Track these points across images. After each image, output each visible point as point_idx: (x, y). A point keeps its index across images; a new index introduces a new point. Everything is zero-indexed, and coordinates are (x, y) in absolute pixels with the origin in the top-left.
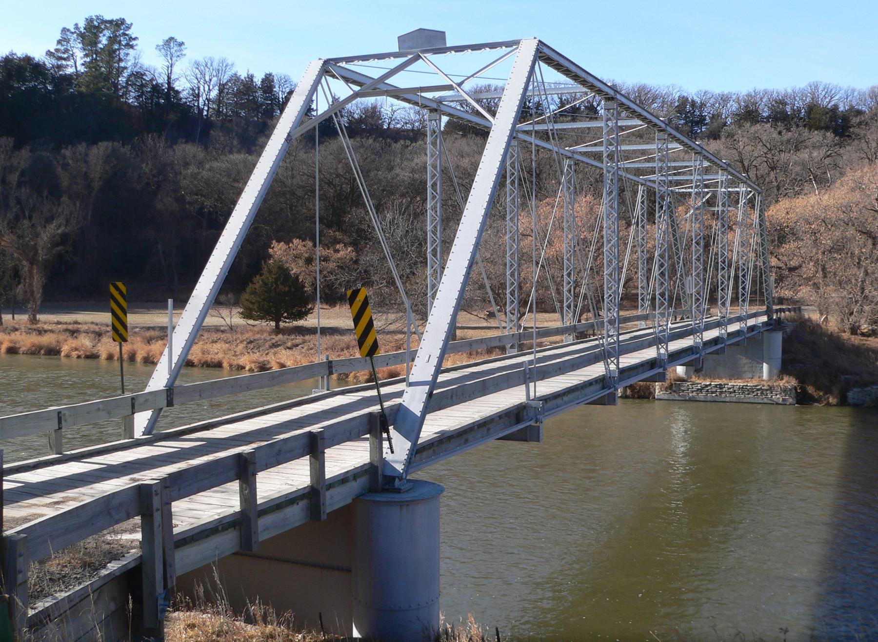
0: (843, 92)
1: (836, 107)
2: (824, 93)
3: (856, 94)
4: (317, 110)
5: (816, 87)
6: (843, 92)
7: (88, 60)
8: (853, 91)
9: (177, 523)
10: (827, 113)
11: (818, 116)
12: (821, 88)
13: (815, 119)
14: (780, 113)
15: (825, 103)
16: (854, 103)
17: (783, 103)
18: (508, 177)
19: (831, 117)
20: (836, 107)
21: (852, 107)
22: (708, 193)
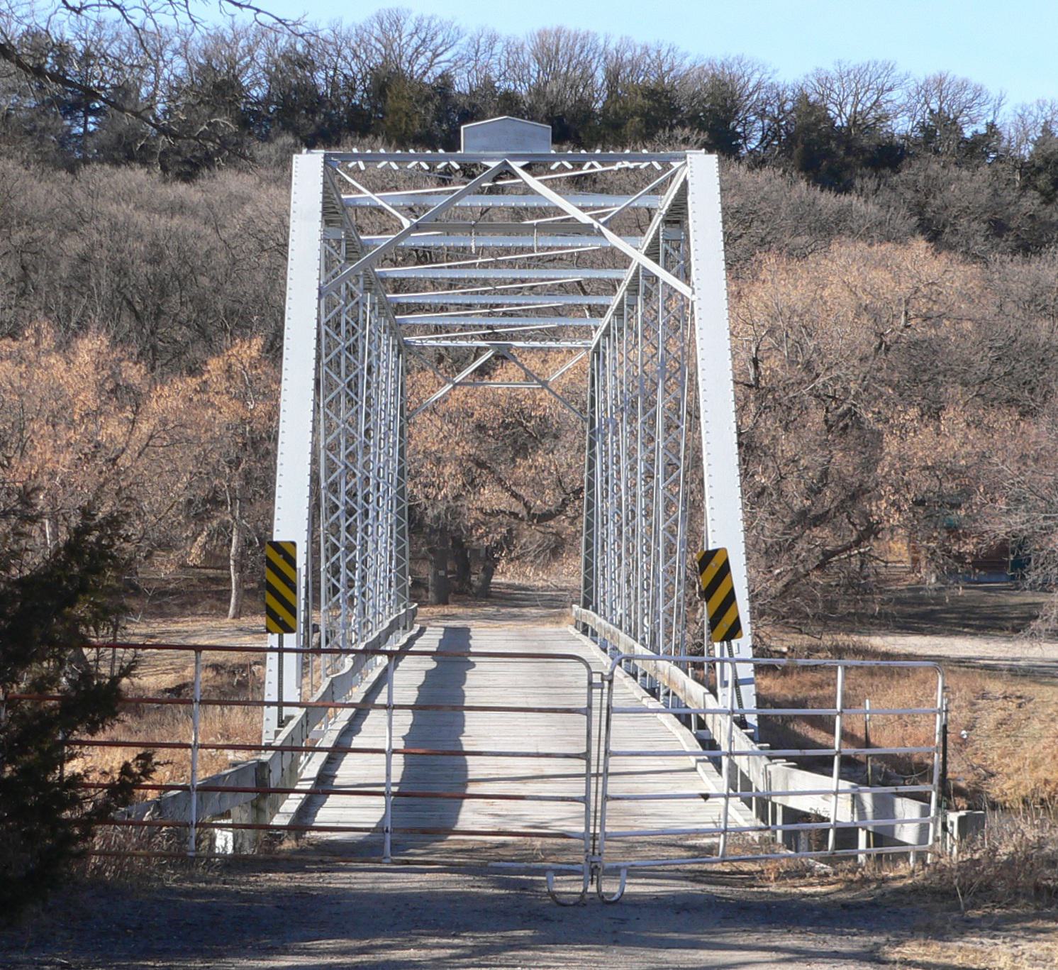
0: (463, 41)
1: (445, 82)
2: (415, 41)
3: (498, 48)
4: (186, 24)
5: (397, 23)
6: (463, 41)
7: (394, 143)
8: (493, 40)
9: (235, 711)
10: (429, 98)
11: (404, 105)
12: (409, 27)
13: (396, 112)
14: (297, 90)
15: (424, 69)
16: (494, 74)
17: (305, 63)
18: (343, 447)
19: (438, 109)
20: (445, 82)
21: (488, 84)
22: (486, 349)
